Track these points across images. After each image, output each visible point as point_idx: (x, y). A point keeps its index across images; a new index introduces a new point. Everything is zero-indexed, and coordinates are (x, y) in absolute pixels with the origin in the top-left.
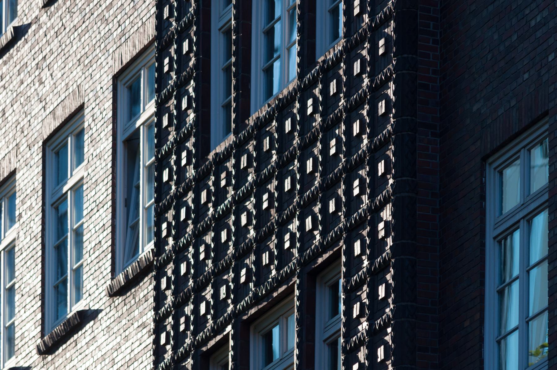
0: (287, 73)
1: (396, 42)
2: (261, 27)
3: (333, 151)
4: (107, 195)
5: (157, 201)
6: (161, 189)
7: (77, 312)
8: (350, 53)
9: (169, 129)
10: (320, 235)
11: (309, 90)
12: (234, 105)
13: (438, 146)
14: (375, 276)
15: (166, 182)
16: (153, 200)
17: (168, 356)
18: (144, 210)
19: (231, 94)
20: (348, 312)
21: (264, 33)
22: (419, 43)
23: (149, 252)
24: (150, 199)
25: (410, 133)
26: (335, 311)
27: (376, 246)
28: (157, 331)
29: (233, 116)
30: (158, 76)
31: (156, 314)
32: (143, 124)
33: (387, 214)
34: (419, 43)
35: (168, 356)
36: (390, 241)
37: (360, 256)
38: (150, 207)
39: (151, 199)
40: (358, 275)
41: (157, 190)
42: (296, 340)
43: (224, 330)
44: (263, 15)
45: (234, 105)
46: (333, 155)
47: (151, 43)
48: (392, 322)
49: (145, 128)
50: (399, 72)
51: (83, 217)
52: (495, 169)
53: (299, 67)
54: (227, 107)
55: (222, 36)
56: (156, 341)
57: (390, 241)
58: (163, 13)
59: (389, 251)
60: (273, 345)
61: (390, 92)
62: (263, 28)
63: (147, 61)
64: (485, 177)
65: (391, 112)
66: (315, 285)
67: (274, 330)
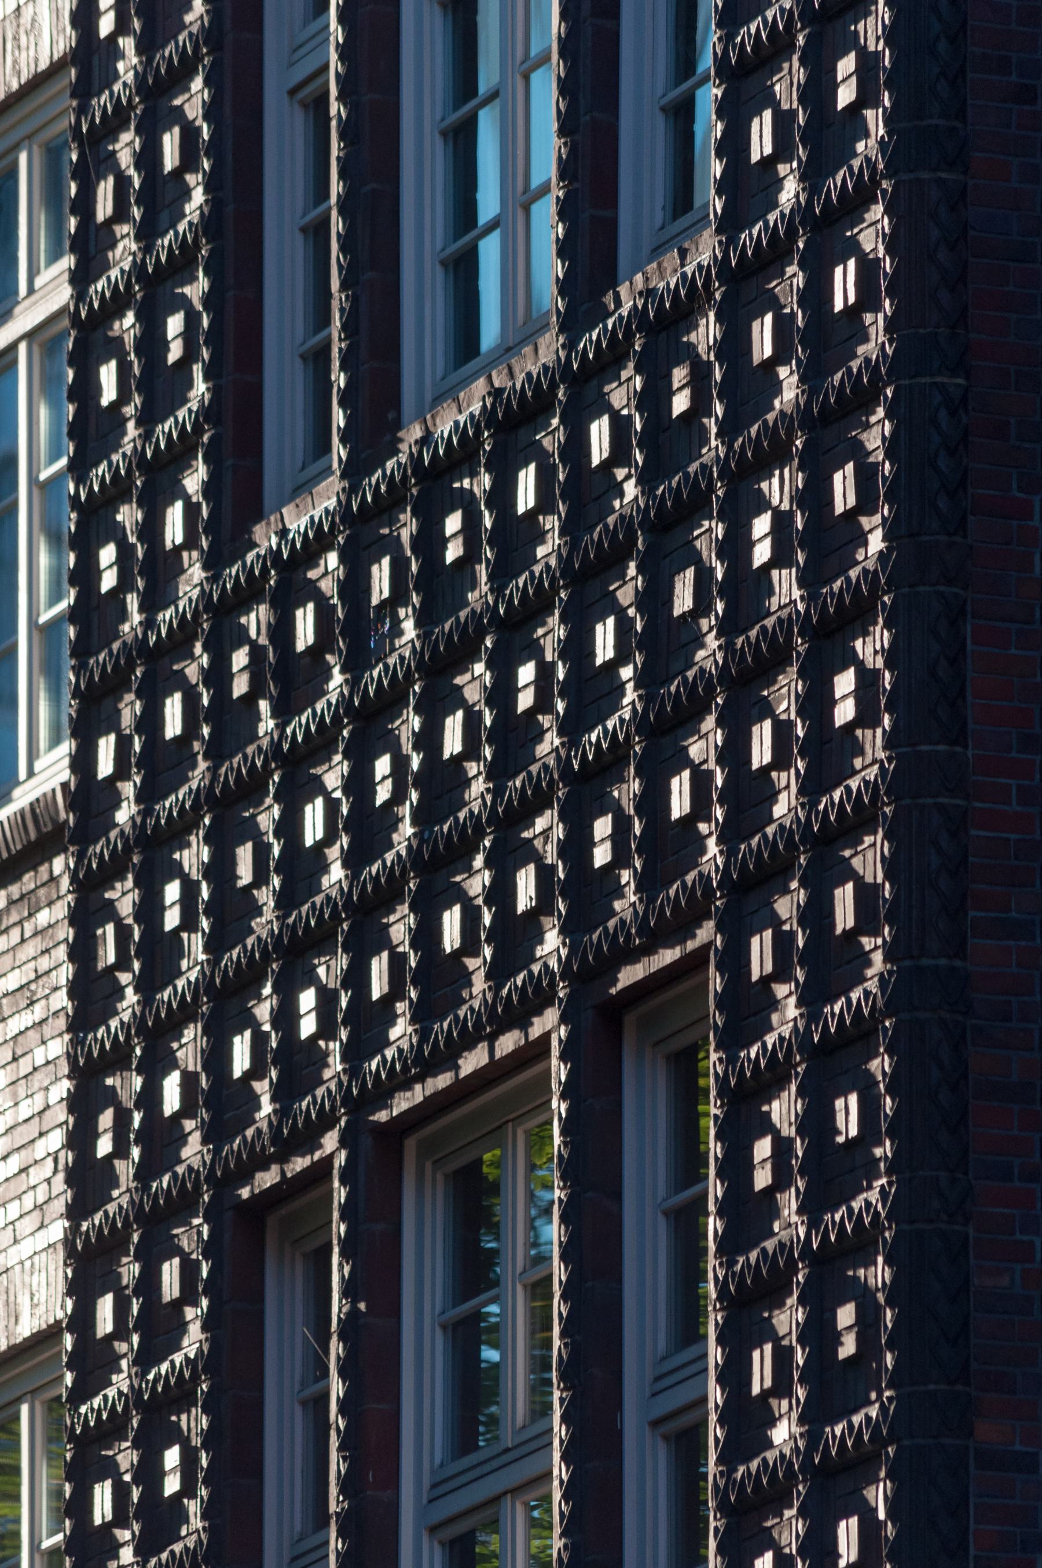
0: (525, 261)
2: (434, 372)
3: (680, 403)
5: (79, 468)
8: (742, 286)
11: (595, 382)
12: (337, 224)
15: (105, 779)
18: (36, 492)
19: (327, 448)
21: (444, 134)
23: (54, 790)
25: (944, 175)
28: (84, 1103)
32: (29, 336)
34: (974, 832)
36: (875, 120)
38: (55, 623)
40: (765, 21)
42: (555, 24)
44: (439, 61)
45: (337, 224)
47: (56, 68)
48: (887, 810)
49: (36, 349)
50: (902, 382)
54: (320, 357)
55: (299, 116)
56: (81, 1138)
57: (875, 120)
58: (94, 202)
60: (480, 18)
61: (873, 440)
62: (438, 117)
63: (50, 116)
65: (877, 308)
66: (620, 1048)
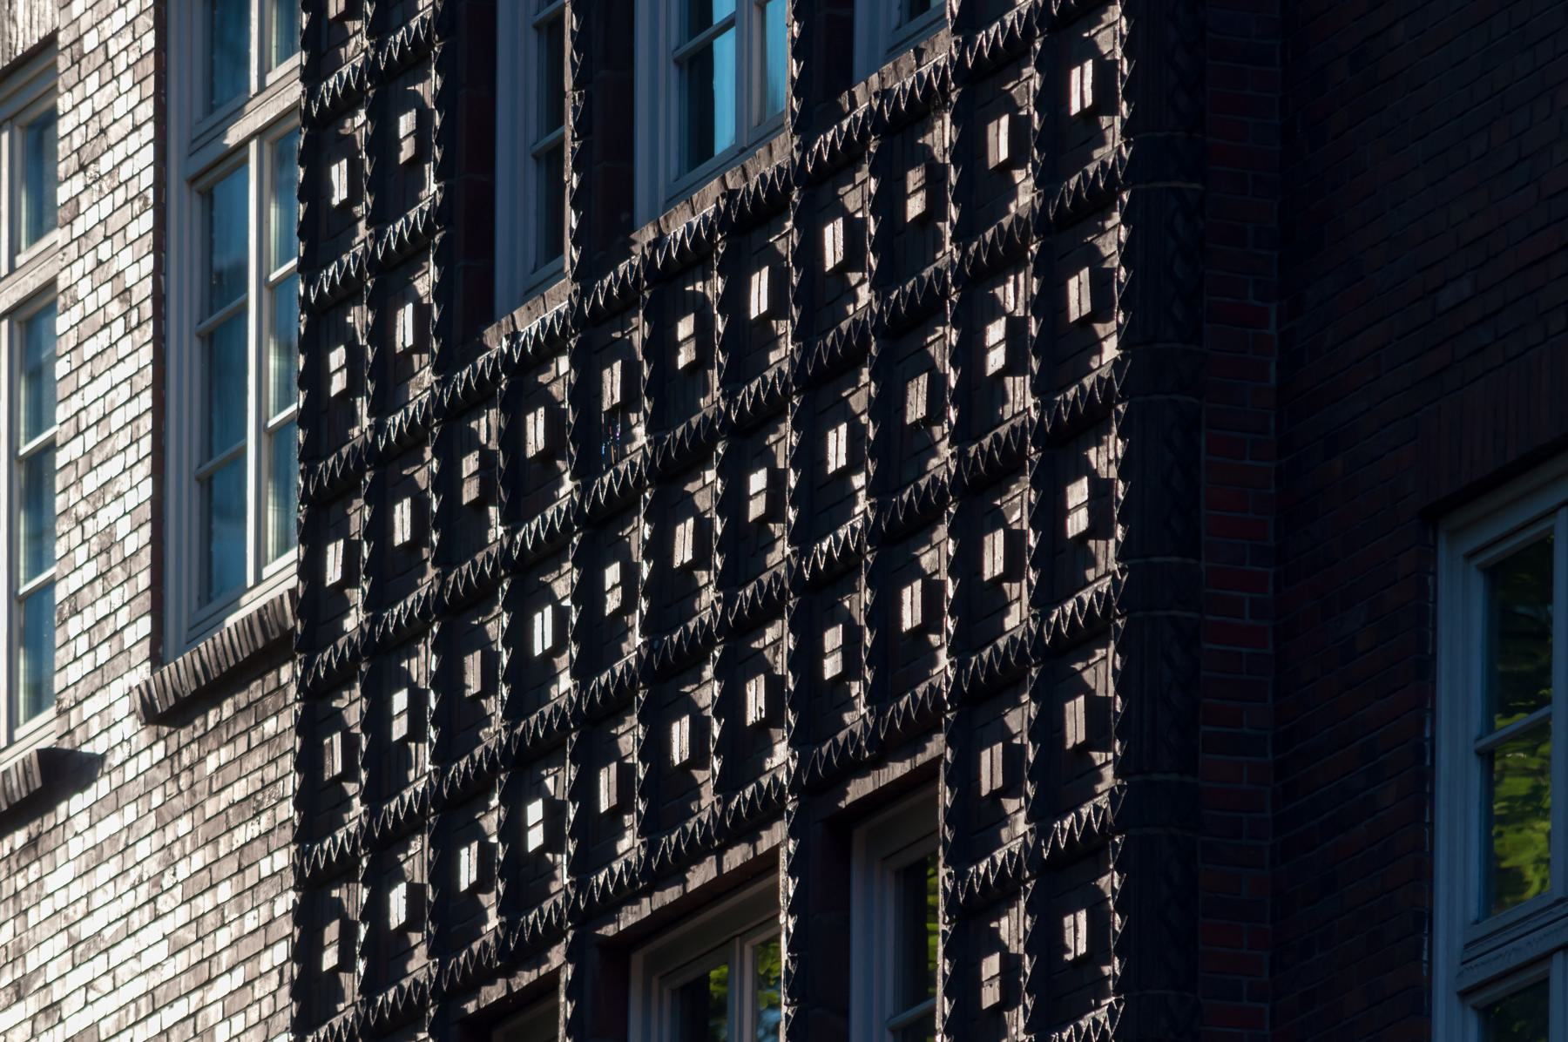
1: (1131, 83)
4: (141, 101)
6: (320, 231)
7: (40, 752)
9: (349, 24)
10: (872, 287)
13: (1272, 330)
14: (1062, 237)
16: (294, 262)
17: (346, 1012)
18: (266, 293)
19: (559, 250)
20: (965, 984)
21: (678, 62)
22: (1207, 646)
24: (283, 404)
26: (917, 981)
27: (1060, 141)
29: (571, 220)
30: (309, 24)
31: (311, 92)
32: (259, 133)
33: (1101, 671)
35: (346, 1012)
37: (1006, 168)
39: (289, 404)
41: (307, 230)
43: (540, 958)
46: (917, 219)
48: (1119, 622)
51: (53, 562)
52: (1470, 556)
53: (796, 93)
59: (1103, 801)
62: (673, 45)
64: (1435, 574)
65: (1114, 111)
67: (717, 43)
